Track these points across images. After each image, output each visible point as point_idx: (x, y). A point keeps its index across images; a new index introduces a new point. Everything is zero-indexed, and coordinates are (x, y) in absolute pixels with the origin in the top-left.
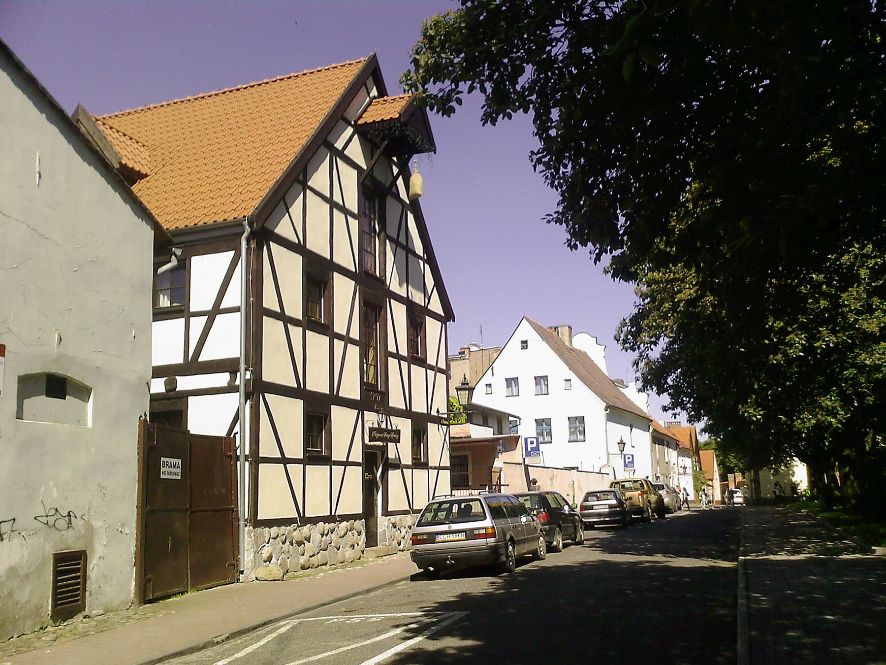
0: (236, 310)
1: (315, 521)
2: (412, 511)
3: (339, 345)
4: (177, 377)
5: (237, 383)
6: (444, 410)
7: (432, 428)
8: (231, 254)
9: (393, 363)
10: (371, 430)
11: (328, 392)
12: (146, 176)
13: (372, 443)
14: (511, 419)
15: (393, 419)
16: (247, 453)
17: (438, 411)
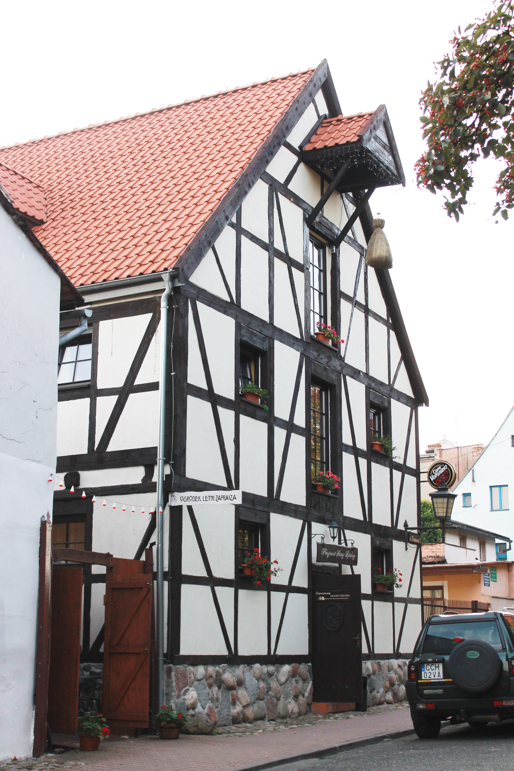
0: (154, 386)
1: (250, 660)
2: (397, 655)
3: (280, 434)
4: (80, 472)
5: (155, 479)
6: (413, 523)
7: (398, 546)
8: (149, 316)
9: (348, 459)
10: (321, 546)
11: (266, 495)
12: (42, 222)
13: (320, 564)
14: (497, 541)
15: (350, 534)
16: (166, 569)
17: (406, 525)
